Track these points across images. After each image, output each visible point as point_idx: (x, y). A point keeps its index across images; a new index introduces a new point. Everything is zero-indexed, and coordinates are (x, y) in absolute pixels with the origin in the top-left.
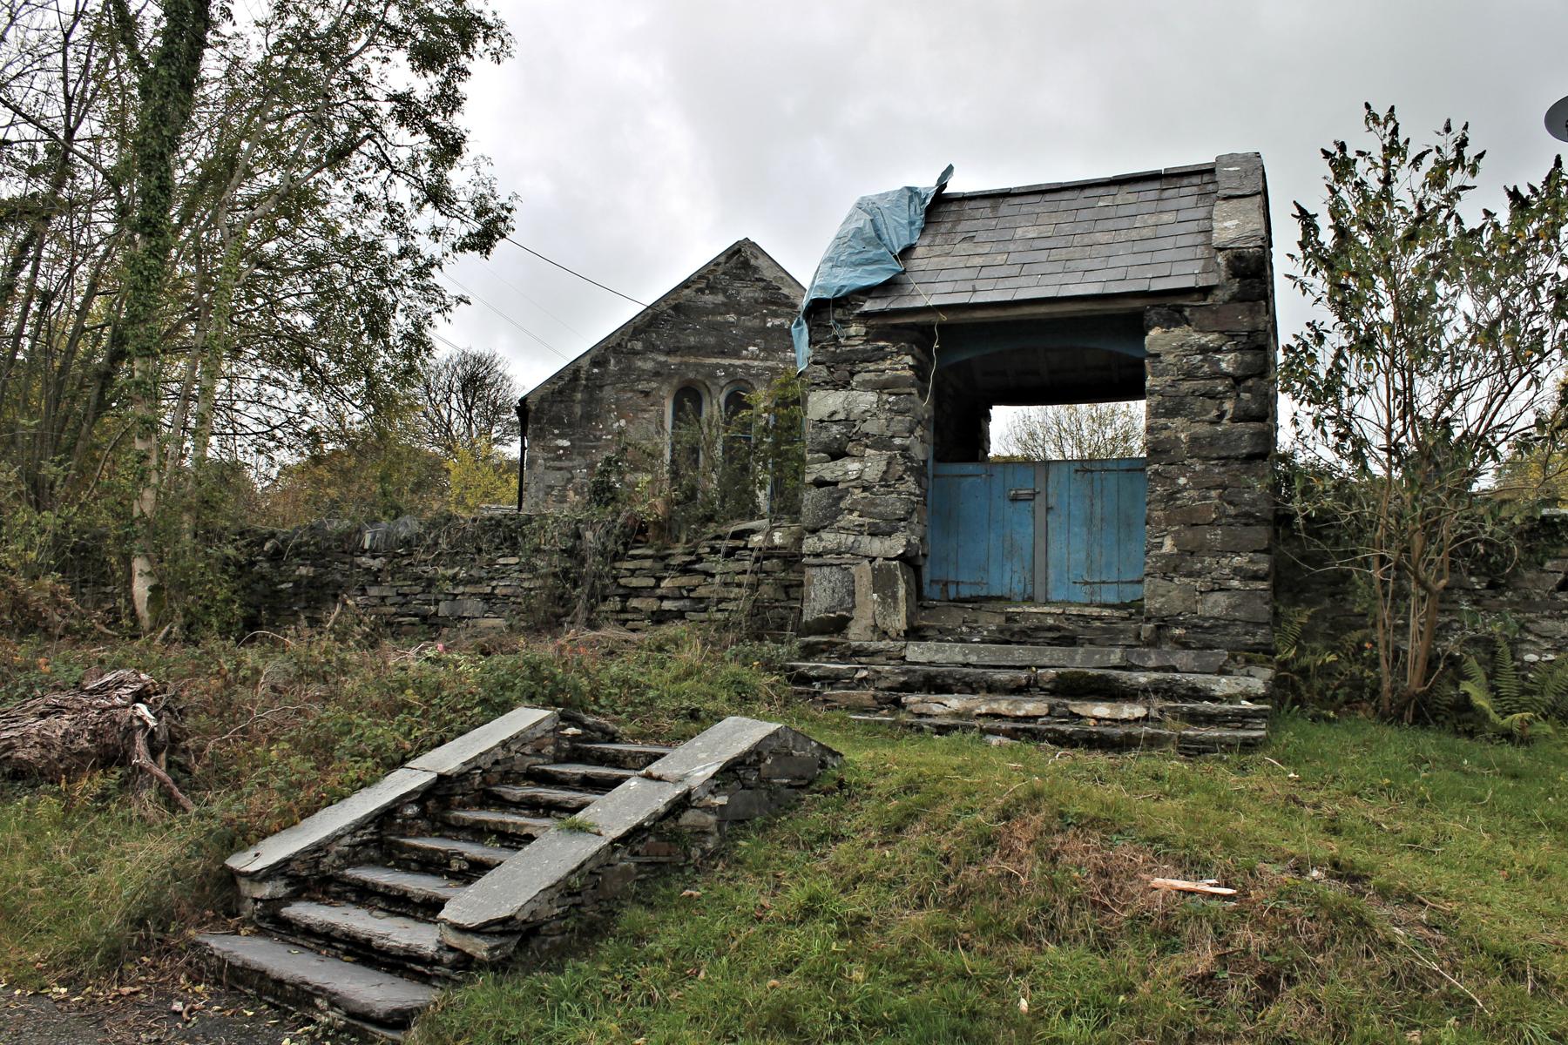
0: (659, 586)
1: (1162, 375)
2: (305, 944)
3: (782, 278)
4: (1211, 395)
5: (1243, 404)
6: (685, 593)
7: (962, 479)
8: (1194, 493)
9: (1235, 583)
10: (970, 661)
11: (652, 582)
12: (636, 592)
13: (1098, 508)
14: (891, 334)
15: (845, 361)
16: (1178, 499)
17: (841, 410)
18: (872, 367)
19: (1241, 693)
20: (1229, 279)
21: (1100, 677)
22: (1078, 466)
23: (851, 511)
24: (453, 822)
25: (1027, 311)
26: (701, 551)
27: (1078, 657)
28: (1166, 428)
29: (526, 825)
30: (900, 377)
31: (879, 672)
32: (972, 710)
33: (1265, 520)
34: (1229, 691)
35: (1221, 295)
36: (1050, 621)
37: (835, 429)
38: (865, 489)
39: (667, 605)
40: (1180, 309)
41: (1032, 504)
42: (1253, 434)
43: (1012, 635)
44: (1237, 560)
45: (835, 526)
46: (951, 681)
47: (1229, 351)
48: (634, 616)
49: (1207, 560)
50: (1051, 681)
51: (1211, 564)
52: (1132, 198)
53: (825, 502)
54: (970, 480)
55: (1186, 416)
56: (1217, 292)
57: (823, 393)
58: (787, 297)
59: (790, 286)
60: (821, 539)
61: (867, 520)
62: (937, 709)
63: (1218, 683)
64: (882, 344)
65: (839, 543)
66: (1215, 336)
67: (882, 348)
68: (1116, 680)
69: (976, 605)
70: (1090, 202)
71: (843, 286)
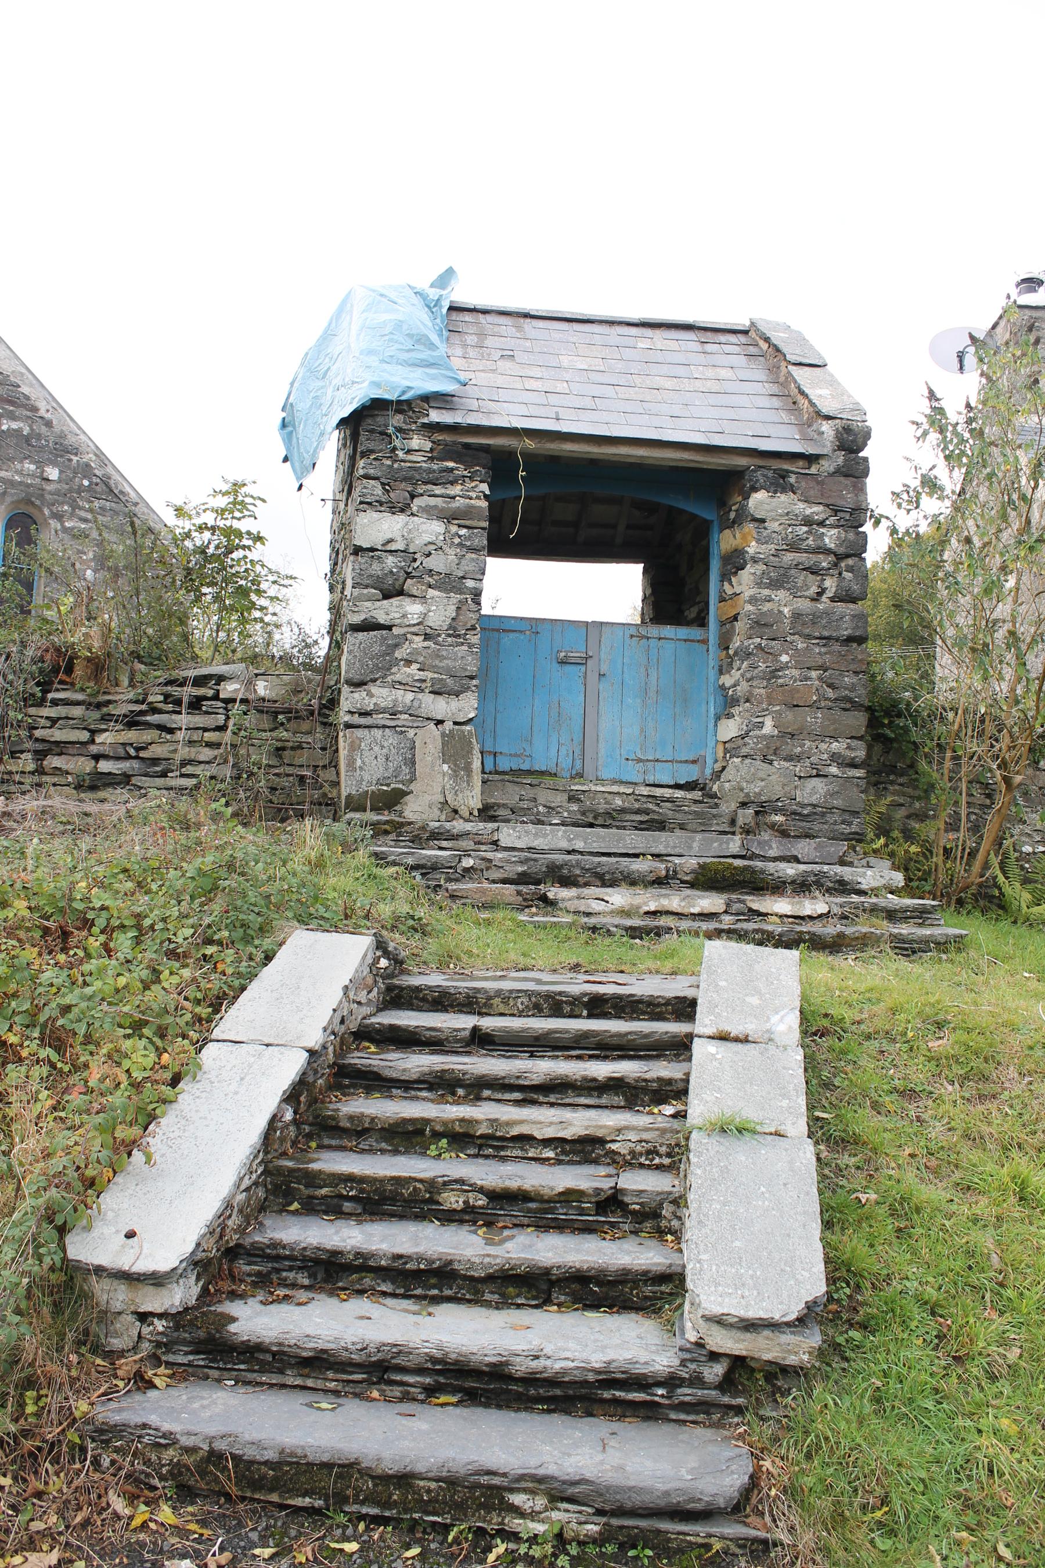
0: (93, 742)
1: (766, 543)
2: (310, 1383)
3: (22, 374)
4: (814, 571)
5: (845, 584)
6: (132, 752)
7: (503, 635)
8: (795, 673)
9: (834, 770)
10: (576, 847)
11: (85, 736)
12: (60, 748)
13: (653, 679)
14: (466, 454)
15: (405, 479)
16: (780, 677)
17: (399, 539)
18: (438, 490)
19: (885, 887)
20: (835, 451)
21: (746, 868)
22: (633, 631)
23: (408, 663)
24: (345, 1124)
25: (623, 450)
26: (151, 699)
27: (695, 845)
28: (769, 600)
29: (521, 1122)
30: (473, 507)
31: (490, 861)
32: (638, 907)
33: (862, 705)
34: (874, 884)
35: (827, 466)
36: (618, 802)
37: (390, 561)
38: (427, 637)
39: (104, 766)
40: (784, 475)
41: (583, 668)
42: (854, 616)
43: (595, 818)
44: (835, 746)
45: (389, 679)
46: (578, 872)
47: (832, 526)
48: (56, 779)
49: (808, 743)
50: (693, 872)
51: (811, 749)
52: (674, 345)
53: (376, 649)
54: (512, 635)
55: (789, 589)
56: (822, 462)
57: (376, 515)
58: (28, 398)
59: (31, 385)
60: (370, 695)
61: (430, 675)
62: (596, 906)
63: (864, 875)
64: (451, 464)
65: (395, 701)
66: (821, 508)
67: (452, 470)
68: (763, 872)
69: (535, 781)
70: (630, 341)
71: (409, 388)
